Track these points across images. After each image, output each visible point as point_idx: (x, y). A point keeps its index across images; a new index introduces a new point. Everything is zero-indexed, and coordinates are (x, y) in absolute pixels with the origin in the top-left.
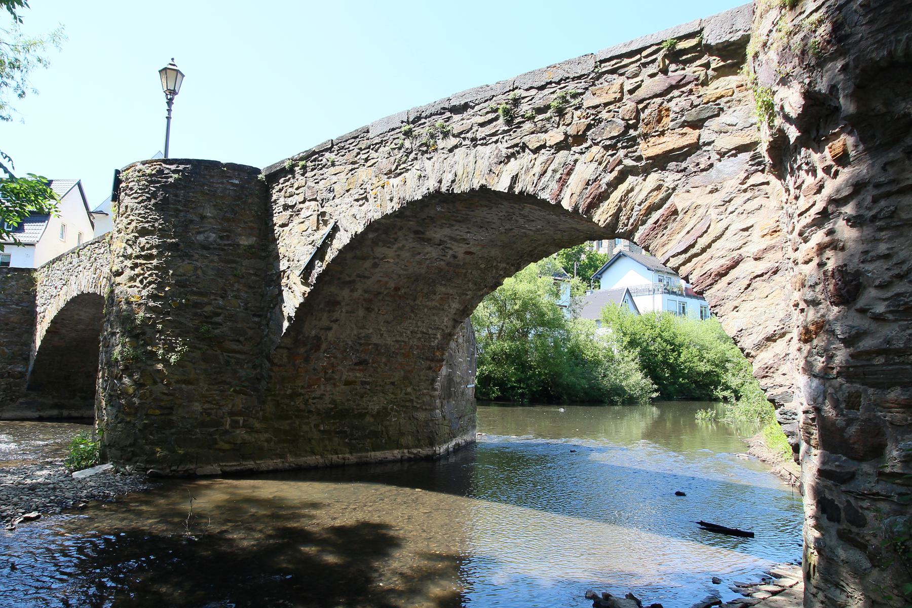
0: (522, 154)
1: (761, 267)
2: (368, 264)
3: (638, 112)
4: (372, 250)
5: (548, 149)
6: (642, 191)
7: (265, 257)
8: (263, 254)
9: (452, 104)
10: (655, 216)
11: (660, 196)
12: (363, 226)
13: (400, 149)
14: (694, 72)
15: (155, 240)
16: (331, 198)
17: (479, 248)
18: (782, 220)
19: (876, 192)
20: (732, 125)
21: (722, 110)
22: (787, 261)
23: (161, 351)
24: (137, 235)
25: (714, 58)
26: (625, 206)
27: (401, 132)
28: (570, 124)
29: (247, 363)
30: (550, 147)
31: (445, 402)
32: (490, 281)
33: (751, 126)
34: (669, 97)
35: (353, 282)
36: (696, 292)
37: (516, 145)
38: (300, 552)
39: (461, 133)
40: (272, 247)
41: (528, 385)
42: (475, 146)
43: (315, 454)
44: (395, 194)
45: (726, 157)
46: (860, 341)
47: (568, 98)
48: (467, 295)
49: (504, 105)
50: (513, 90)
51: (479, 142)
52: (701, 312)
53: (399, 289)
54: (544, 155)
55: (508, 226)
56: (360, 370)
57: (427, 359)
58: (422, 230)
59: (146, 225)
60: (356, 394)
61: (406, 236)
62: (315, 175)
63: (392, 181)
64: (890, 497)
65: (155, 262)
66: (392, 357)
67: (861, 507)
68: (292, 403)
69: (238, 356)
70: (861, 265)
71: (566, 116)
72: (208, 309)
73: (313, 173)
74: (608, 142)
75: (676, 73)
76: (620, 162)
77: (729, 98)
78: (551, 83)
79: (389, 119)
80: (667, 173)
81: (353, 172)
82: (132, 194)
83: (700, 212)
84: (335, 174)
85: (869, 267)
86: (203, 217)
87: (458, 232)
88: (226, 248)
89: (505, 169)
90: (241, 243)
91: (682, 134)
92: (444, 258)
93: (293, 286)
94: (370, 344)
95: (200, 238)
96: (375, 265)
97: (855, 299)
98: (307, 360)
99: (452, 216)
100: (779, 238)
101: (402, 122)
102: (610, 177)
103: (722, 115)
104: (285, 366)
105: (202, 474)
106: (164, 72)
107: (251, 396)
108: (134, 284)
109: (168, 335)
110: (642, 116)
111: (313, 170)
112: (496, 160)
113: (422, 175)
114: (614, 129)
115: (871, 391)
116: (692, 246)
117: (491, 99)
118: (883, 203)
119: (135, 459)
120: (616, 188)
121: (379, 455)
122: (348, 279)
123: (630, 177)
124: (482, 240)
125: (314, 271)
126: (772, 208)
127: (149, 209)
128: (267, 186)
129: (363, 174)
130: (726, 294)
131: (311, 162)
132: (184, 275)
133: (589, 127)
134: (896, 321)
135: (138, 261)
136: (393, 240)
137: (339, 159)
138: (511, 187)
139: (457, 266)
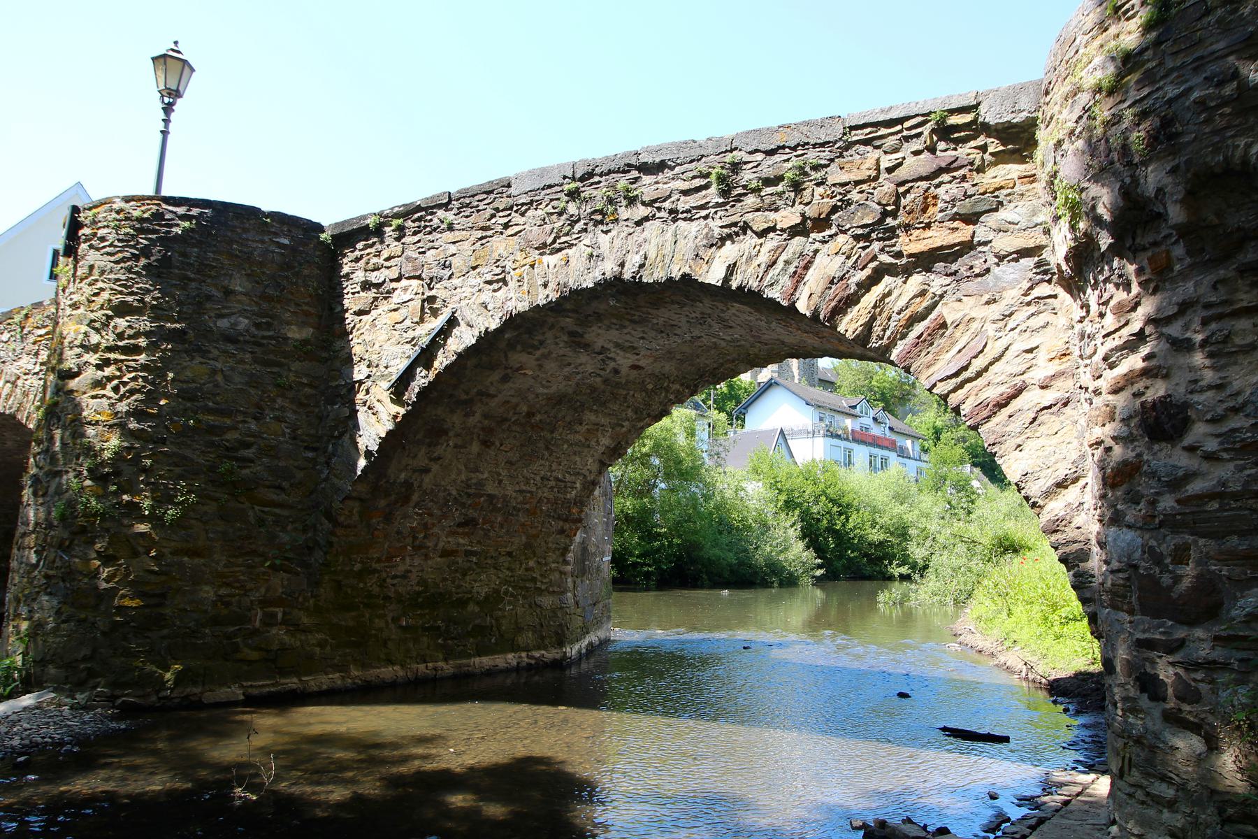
0: (742, 237)
1: (1048, 397)
2: (496, 376)
3: (898, 196)
4: (506, 356)
5: (778, 232)
6: (902, 297)
7: (326, 360)
8: (324, 355)
9: (642, 161)
10: (919, 328)
11: (925, 304)
12: (498, 321)
13: (560, 214)
14: (968, 155)
15: (145, 324)
16: (446, 277)
17: (651, 360)
18: (1072, 342)
19: (1205, 313)
20: (1013, 223)
21: (1001, 203)
22: (1079, 390)
23: (147, 503)
24: (110, 313)
25: (992, 140)
26: (880, 314)
27: (562, 191)
28: (810, 203)
29: (292, 522)
30: (782, 230)
31: (578, 581)
32: (656, 408)
33: (1035, 226)
34: (937, 181)
35: (469, 402)
36: (969, 427)
37: (735, 224)
38: (446, 805)
39: (655, 201)
40: (338, 344)
41: (655, 562)
42: (675, 220)
43: (393, 664)
44: (550, 277)
45: (1005, 262)
46: (1188, 484)
47: (807, 169)
48: (623, 426)
49: (718, 170)
50: (731, 151)
51: (680, 216)
52: (871, 463)
53: (533, 414)
54: (773, 241)
55: (696, 333)
56: (465, 534)
57: (559, 518)
58: (579, 330)
59: (129, 299)
60: (456, 571)
61: (556, 338)
62: (419, 241)
63: (546, 259)
64: (1229, 664)
65: (142, 358)
66: (513, 515)
67: (1195, 680)
68: (361, 585)
69: (277, 511)
70: (1189, 396)
71: (805, 193)
72: (232, 436)
73: (416, 238)
74: (860, 231)
75: (946, 153)
76: (874, 258)
77: (1009, 191)
78: (784, 147)
79: (543, 172)
80: (933, 276)
81: (484, 241)
82: (104, 247)
83: (975, 326)
84: (454, 243)
85: (1196, 398)
86: (228, 293)
87: (628, 337)
88: (265, 342)
89: (718, 255)
90: (290, 335)
91: (953, 229)
92: (602, 373)
93: (377, 405)
94: (482, 496)
95: (223, 323)
96: (505, 379)
97: (1181, 436)
98: (388, 518)
99: (628, 314)
100: (1069, 363)
101: (565, 178)
102: (861, 275)
103: (1001, 210)
104: (355, 527)
105: (212, 701)
106: (162, 60)
107: (297, 574)
108: (102, 392)
109: (161, 477)
110: (903, 202)
111: (415, 233)
112: (705, 242)
113: (595, 254)
114: (868, 215)
115: (1201, 542)
116: (965, 368)
117: (698, 160)
118: (1214, 326)
119: (91, 683)
120: (868, 290)
121: (486, 661)
122: (464, 397)
123: (886, 277)
124: (657, 350)
125: (413, 384)
126: (1060, 326)
127: (135, 273)
128: (334, 252)
129: (499, 245)
130: (1008, 429)
131: (414, 221)
132: (194, 381)
133: (835, 209)
134: (1231, 460)
135: (112, 356)
136: (536, 343)
137: (459, 221)
138: (726, 280)
139: (618, 385)
